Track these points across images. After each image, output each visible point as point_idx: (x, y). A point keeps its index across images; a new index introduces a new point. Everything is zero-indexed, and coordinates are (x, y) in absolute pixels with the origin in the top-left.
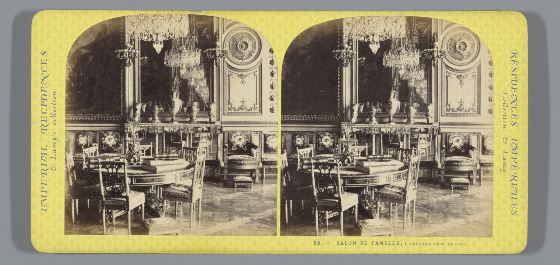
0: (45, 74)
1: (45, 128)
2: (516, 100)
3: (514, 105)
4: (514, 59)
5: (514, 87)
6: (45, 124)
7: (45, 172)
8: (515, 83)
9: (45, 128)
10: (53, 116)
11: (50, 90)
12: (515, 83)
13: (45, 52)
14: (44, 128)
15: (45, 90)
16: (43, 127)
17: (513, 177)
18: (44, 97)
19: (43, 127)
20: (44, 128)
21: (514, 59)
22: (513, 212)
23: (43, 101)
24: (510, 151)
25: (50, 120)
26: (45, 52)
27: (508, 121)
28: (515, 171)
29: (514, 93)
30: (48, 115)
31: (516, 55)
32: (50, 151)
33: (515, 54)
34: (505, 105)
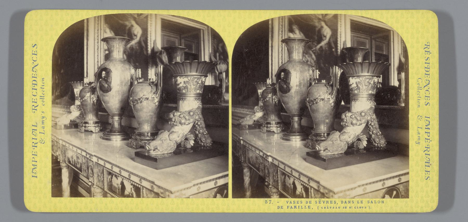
5: (427, 73)
6: (36, 105)
7: (36, 145)
8: (428, 70)
10: (42, 98)
12: (428, 70)
13: (35, 45)
16: (33, 107)
17: (426, 149)
18: (34, 82)
20: (35, 108)
23: (33, 85)
26: (35, 45)
27: (423, 102)
29: (428, 79)
31: (428, 47)
32: (39, 129)
33: (427, 46)
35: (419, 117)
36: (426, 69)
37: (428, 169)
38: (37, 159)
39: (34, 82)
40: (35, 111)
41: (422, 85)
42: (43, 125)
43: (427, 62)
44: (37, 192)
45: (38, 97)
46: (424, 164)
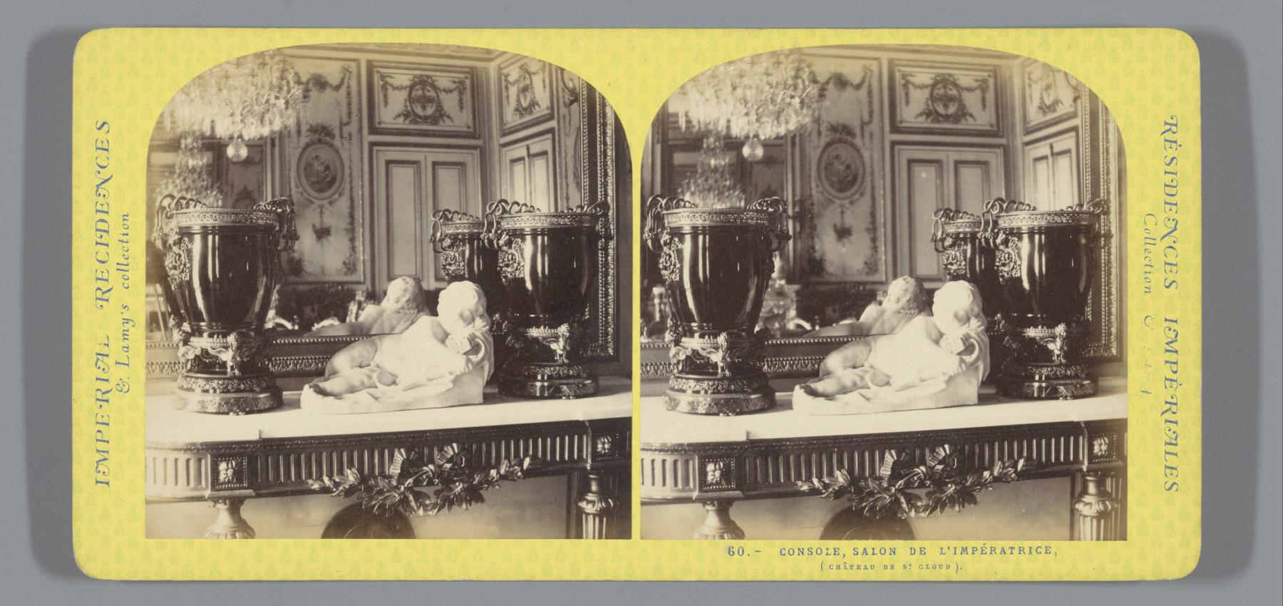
1: (106, 296)
2: (1175, 229)
3: (1168, 241)
4: (1169, 136)
11: (113, 219)
12: (1173, 191)
13: (104, 124)
14: (103, 296)
15: (105, 208)
18: (102, 226)
20: (103, 296)
23: (99, 234)
25: (115, 277)
29: (1172, 215)
30: (112, 265)
31: (1174, 129)
32: (115, 350)
33: (1171, 126)
36: (1169, 190)
37: (1172, 461)
38: (108, 433)
39: (102, 226)
40: (104, 404)
43: (1169, 169)
45: (112, 265)
46: (1164, 448)
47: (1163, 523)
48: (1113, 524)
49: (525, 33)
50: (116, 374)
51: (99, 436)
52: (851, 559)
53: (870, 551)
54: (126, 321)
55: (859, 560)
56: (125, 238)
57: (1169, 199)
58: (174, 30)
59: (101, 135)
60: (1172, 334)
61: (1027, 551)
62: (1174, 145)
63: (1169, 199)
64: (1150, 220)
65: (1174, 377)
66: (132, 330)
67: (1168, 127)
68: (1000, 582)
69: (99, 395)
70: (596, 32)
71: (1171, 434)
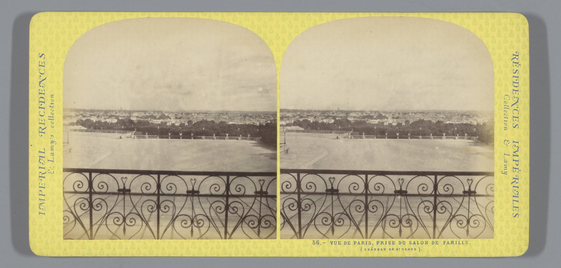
0: (43, 77)
2: (518, 102)
3: (515, 107)
4: (515, 60)
9: (43, 131)
10: (51, 118)
12: (516, 85)
13: (43, 54)
14: (42, 131)
17: (514, 180)
18: (42, 100)
19: (41, 130)
20: (42, 131)
21: (515, 60)
22: (514, 215)
23: (41, 103)
24: (511, 154)
25: (48, 123)
26: (43, 54)
27: (510, 125)
28: (516, 173)
29: (516, 95)
30: (46, 117)
32: (48, 155)
33: (516, 56)
34: (506, 107)
35: (506, 142)
37: (516, 204)
39: (42, 100)
41: (510, 102)
42: (52, 152)
43: (515, 75)
44: (47, 229)
45: (46, 117)
46: (511, 199)
47: (509, 232)
48: (489, 230)
49: (225, 14)
50: (48, 165)
51: (40, 193)
52: (376, 246)
53: (416, 243)
54: (52, 142)
55: (412, 246)
56: (52, 105)
57: (42, 96)
58: (82, 12)
59: (42, 60)
60: (516, 148)
61: (365, 243)
62: (517, 65)
63: (42, 96)
64: (507, 98)
65: (517, 167)
66: (55, 145)
67: (514, 56)
68: (477, 257)
69: (41, 175)
70: (282, 14)
71: (515, 192)
